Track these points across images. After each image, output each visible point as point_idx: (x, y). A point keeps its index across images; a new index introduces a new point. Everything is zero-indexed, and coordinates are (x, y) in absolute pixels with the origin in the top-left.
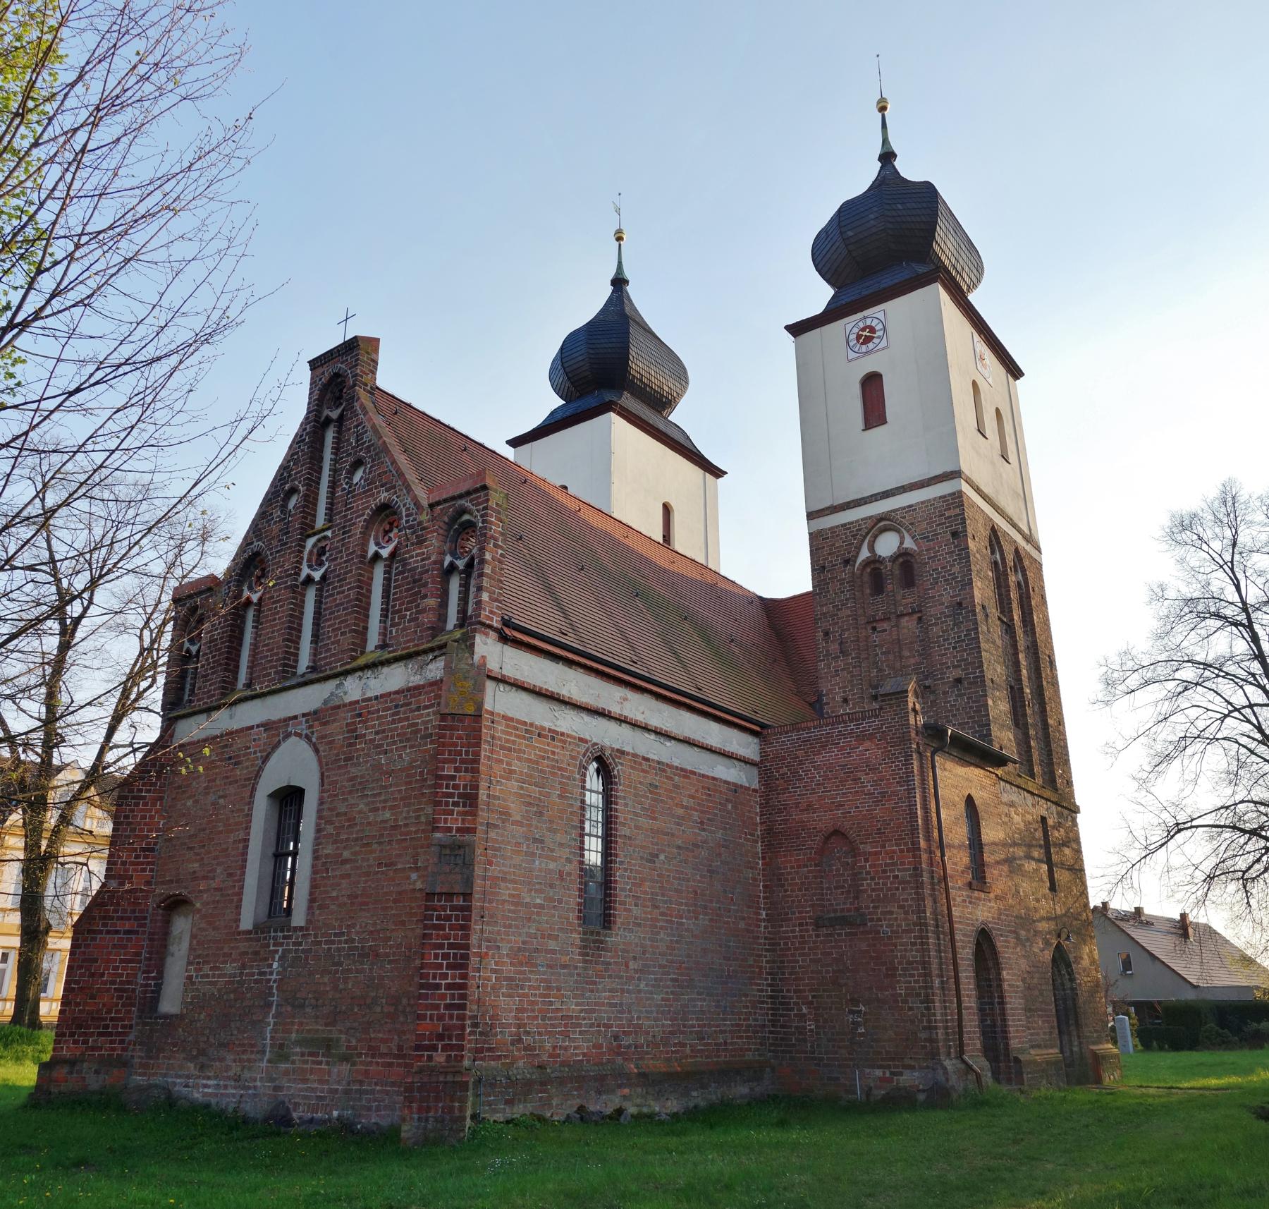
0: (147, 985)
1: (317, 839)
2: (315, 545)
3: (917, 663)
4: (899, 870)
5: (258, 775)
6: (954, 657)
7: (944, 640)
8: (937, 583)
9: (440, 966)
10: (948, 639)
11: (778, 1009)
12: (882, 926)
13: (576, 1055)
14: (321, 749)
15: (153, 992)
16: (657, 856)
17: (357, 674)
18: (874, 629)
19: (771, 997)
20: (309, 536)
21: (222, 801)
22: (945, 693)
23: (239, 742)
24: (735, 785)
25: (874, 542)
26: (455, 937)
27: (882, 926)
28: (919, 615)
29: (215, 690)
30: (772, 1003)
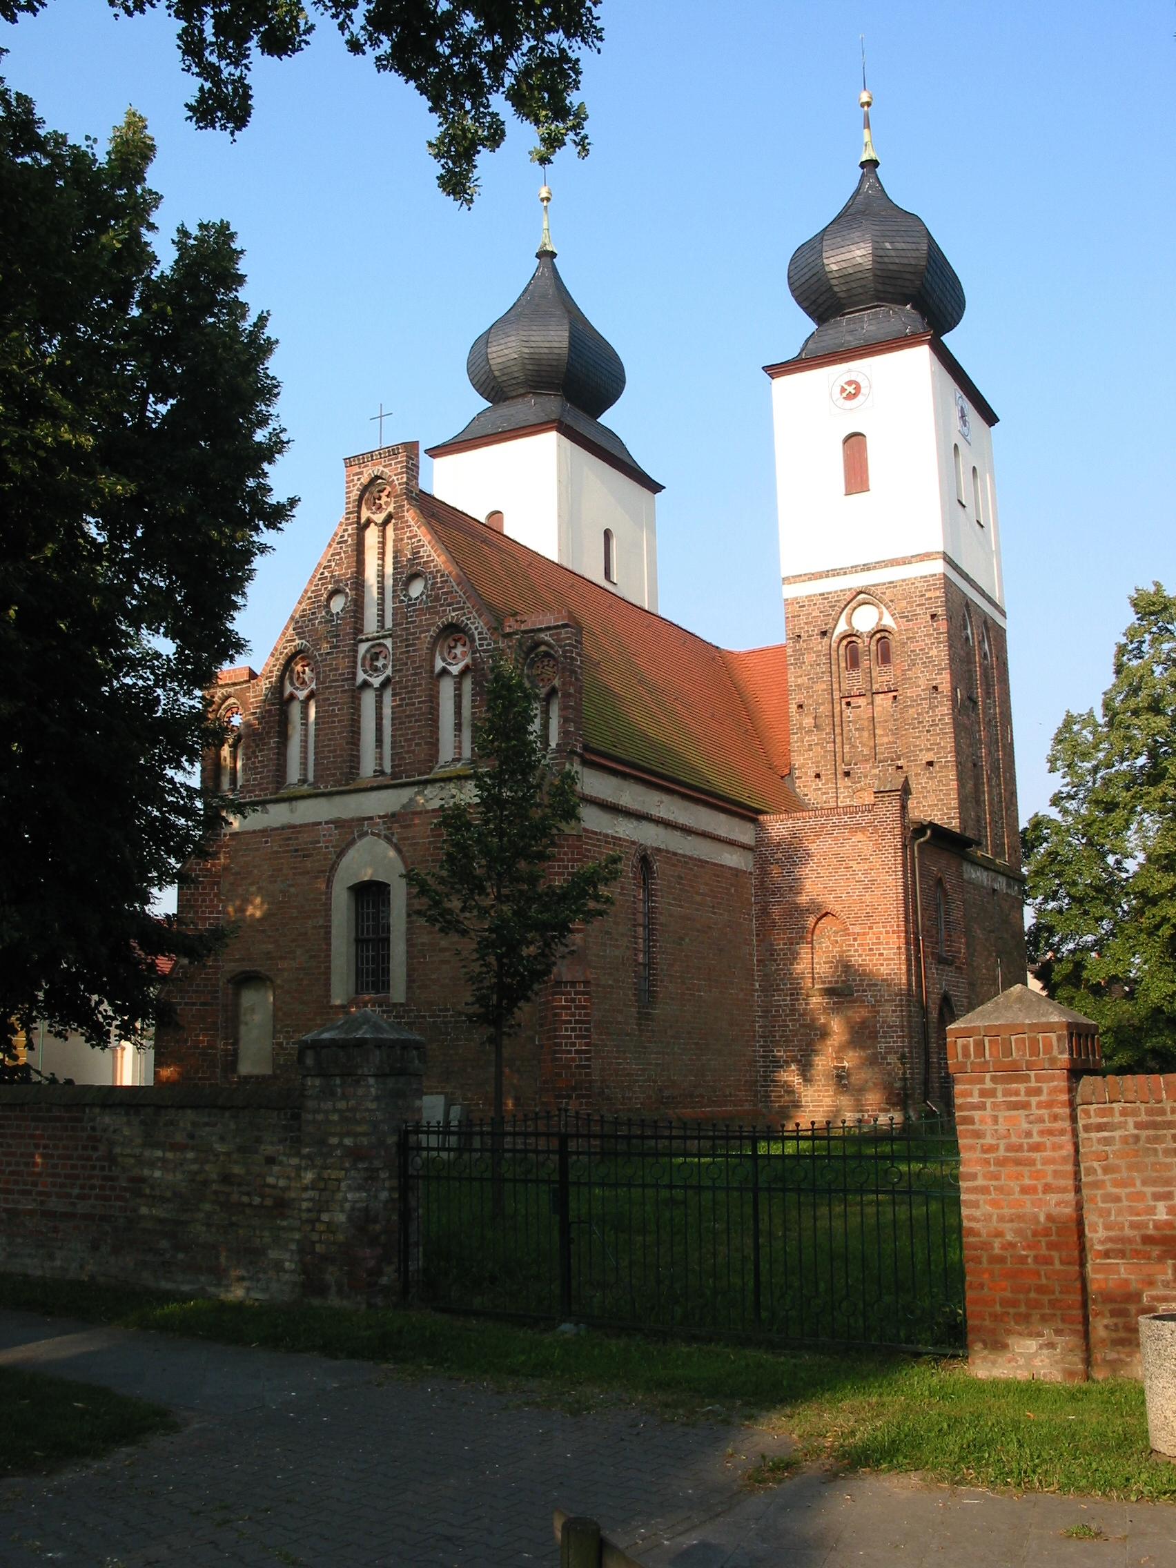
0: (226, 1050)
1: (408, 929)
2: (367, 651)
3: (890, 743)
4: (884, 949)
5: (334, 868)
6: (928, 740)
7: (919, 723)
8: (914, 665)
9: (570, 1037)
10: (922, 722)
11: (769, 1066)
12: (867, 996)
13: (636, 1104)
14: (405, 849)
15: (232, 1055)
16: (683, 939)
17: (438, 785)
18: (848, 704)
19: (763, 1057)
20: (362, 641)
21: (292, 890)
22: (916, 775)
23: (1121, 1059)
24: (736, 870)
25: (852, 614)
26: (580, 1015)
27: (867, 996)
28: (895, 694)
29: (267, 783)
30: (764, 1062)
